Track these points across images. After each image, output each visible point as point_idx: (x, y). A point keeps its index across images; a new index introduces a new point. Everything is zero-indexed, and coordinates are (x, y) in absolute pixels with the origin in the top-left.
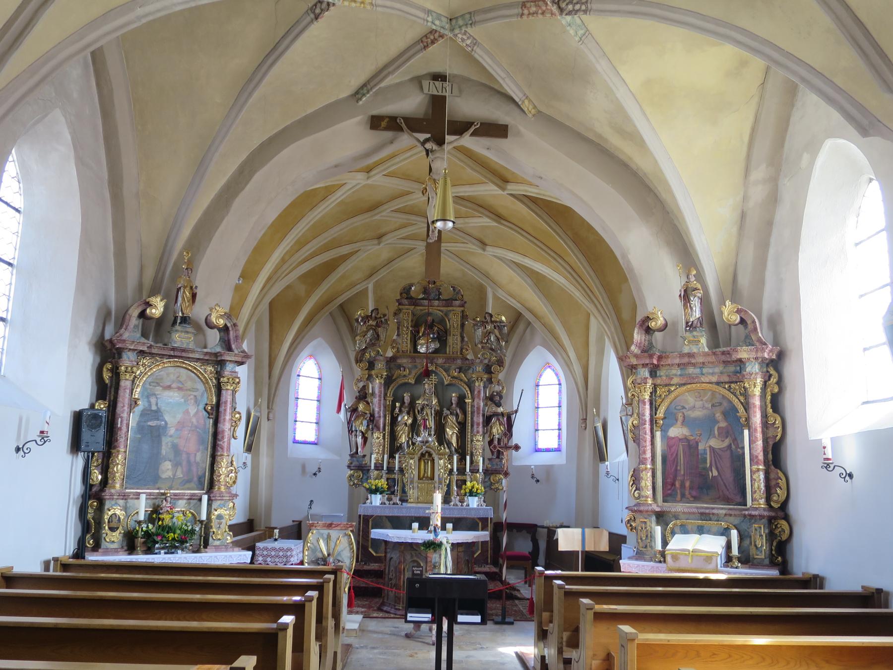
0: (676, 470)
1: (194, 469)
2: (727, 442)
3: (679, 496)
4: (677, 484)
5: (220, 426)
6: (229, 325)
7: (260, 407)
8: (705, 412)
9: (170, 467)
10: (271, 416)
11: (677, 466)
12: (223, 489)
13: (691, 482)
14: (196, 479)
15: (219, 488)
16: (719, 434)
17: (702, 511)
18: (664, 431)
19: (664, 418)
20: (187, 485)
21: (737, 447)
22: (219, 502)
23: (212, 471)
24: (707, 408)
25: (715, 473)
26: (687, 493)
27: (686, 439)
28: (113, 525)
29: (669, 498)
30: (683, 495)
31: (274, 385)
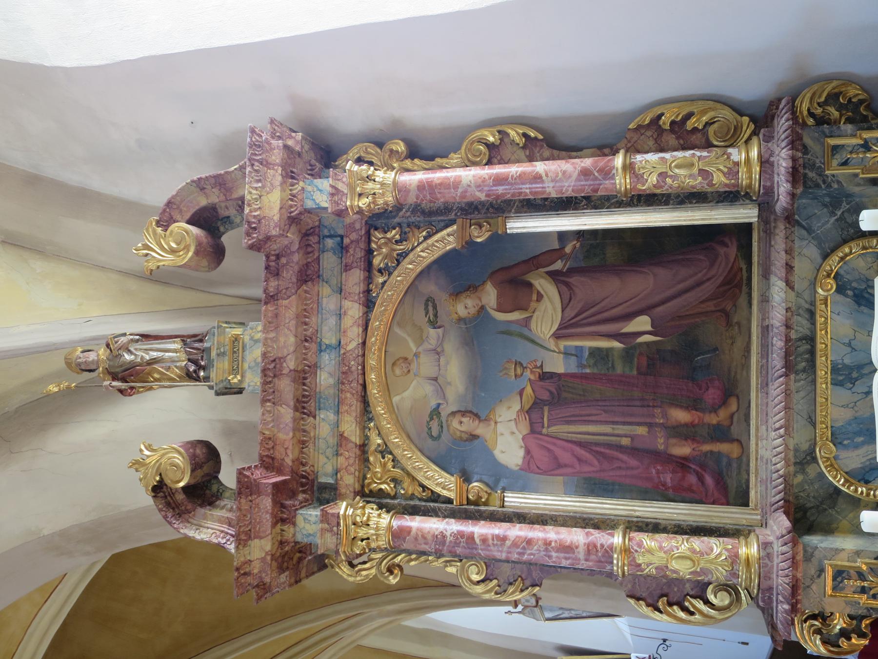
0: (633, 451)
2: (543, 284)
3: (723, 447)
4: (683, 450)
16: (524, 309)
17: (777, 361)
19: (466, 478)
21: (557, 254)
24: (441, 341)
25: (642, 323)
26: (712, 419)
27: (532, 412)
29: (732, 484)
30: (721, 434)
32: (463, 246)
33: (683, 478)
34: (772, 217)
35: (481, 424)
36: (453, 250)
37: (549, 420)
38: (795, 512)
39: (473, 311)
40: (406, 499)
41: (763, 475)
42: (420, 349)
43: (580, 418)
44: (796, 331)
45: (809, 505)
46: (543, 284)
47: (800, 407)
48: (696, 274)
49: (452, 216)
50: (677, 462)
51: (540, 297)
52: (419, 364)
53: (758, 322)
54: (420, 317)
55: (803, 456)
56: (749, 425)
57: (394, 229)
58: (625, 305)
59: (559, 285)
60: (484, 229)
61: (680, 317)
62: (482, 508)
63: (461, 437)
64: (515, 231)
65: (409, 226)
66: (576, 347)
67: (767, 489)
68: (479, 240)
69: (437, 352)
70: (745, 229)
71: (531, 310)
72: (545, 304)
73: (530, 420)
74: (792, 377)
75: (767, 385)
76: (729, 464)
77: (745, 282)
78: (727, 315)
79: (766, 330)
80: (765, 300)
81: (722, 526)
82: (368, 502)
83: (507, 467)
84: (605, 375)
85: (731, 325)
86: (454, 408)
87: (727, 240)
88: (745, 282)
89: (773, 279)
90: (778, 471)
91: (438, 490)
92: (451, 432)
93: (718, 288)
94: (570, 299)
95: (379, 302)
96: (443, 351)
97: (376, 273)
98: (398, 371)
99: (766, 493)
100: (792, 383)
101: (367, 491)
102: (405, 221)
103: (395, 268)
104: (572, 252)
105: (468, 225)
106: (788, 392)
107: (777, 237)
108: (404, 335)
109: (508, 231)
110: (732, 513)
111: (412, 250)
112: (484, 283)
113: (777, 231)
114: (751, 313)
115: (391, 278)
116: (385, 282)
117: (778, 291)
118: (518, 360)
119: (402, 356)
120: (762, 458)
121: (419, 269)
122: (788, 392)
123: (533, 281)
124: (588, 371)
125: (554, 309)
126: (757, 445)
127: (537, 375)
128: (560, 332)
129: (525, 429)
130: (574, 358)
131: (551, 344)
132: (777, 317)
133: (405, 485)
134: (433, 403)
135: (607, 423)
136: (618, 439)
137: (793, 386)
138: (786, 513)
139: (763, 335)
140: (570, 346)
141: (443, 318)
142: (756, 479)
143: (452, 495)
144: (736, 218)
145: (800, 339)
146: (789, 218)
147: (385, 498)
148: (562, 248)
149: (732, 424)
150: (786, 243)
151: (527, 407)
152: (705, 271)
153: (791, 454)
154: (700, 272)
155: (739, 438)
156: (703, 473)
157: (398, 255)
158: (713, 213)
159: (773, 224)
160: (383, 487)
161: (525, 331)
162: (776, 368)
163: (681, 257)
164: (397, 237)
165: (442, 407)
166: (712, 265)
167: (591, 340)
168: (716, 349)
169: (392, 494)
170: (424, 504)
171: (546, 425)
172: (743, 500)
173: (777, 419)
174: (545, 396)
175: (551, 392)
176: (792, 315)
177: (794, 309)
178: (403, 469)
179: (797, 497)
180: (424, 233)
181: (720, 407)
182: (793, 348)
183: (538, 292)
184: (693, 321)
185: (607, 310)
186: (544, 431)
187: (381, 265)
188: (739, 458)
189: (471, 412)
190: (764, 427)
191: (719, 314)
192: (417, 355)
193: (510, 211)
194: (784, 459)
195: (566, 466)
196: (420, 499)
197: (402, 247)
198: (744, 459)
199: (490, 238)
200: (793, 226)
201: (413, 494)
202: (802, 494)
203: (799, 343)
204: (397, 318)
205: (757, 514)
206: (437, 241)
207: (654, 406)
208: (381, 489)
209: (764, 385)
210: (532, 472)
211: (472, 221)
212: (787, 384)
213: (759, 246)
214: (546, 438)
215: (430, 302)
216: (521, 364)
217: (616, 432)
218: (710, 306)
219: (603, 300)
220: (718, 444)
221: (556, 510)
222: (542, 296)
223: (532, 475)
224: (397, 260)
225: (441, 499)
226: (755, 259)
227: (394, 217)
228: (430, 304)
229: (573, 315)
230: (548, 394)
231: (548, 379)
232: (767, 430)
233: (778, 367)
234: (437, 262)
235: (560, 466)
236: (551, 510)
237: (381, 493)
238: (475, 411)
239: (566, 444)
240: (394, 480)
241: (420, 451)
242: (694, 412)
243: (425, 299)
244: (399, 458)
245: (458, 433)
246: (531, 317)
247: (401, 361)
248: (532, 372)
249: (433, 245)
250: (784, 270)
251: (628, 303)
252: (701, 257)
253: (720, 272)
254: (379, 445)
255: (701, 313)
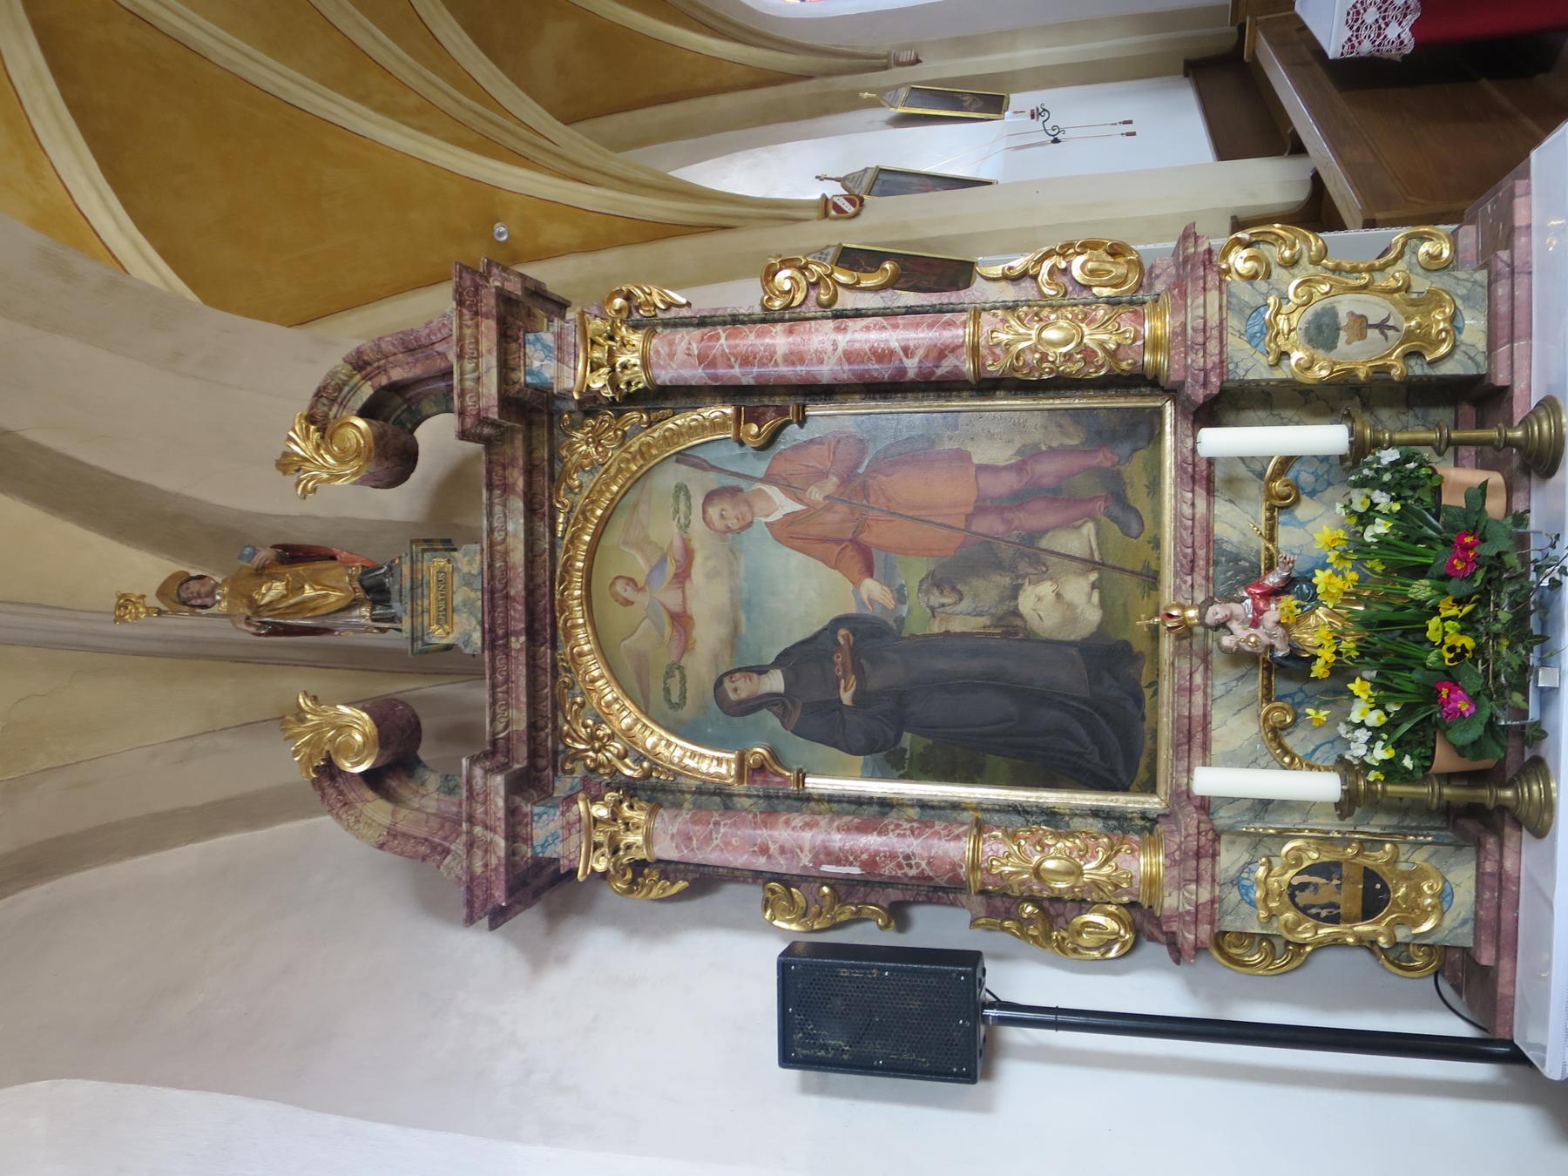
1: (1049, 469)
5: (826, 372)
6: (367, 391)
7: (882, 92)
9: (1046, 589)
10: (906, 56)
12: (1158, 325)
14: (1103, 459)
15: (1156, 345)
20: (1137, 496)
22: (1235, 344)
23: (1061, 384)
28: (1349, 896)
31: (826, 61)
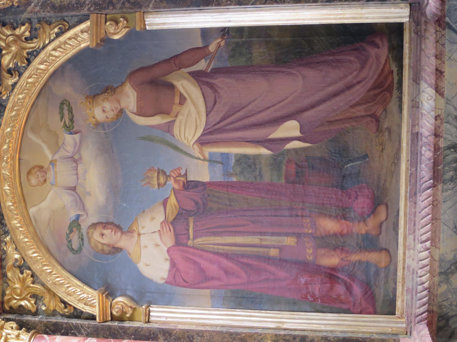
0: (281, 262)
2: (185, 86)
3: (372, 257)
4: (331, 260)
8: (89, 154)
11: (268, 259)
13: (324, 213)
16: (166, 112)
17: (425, 172)
18: (147, 294)
19: (110, 292)
21: (200, 52)
24: (78, 148)
25: (291, 128)
26: (360, 229)
27: (178, 223)
29: (380, 293)
30: (370, 243)
32: (98, 44)
33: (332, 288)
34: (423, 19)
35: (124, 237)
36: (87, 49)
37: (195, 231)
38: (439, 321)
39: (111, 115)
40: (48, 315)
41: (409, 284)
42: (57, 157)
43: (227, 229)
44: (445, 139)
45: (451, 314)
46: (185, 86)
47: (447, 217)
48: (346, 76)
49: (85, 11)
50: (326, 273)
51: (183, 100)
52: (56, 173)
53: (408, 128)
54: (55, 122)
55: (448, 266)
56: (397, 234)
57: (23, 24)
58: (272, 109)
59: (203, 87)
60: (120, 25)
61: (330, 122)
62: (127, 324)
63: (103, 250)
64: (155, 28)
65: (39, 22)
66: (222, 154)
67: (412, 298)
68: (116, 37)
69: (75, 160)
70: (396, 29)
71: (174, 113)
72: (189, 107)
73: (174, 232)
74: (440, 187)
75: (415, 194)
76: (377, 273)
77: (395, 85)
78: (377, 120)
79: (415, 137)
80: (415, 105)
81: (367, 336)
82: (8, 320)
83: (152, 281)
84: (252, 183)
85: (381, 131)
86: (94, 220)
87: (378, 40)
88: (395, 85)
89: (424, 85)
90: (423, 283)
91: (80, 306)
92: (93, 244)
93: (370, 90)
94: (215, 103)
95: (9, 106)
96: (81, 158)
97: (5, 74)
98: (34, 181)
99: (412, 302)
100: (439, 193)
101: (7, 308)
102: (35, 16)
103: (26, 68)
104: (217, 50)
105: (103, 21)
106: (435, 203)
107: (427, 41)
108: (39, 142)
109: (148, 28)
110: (378, 322)
111: (44, 47)
112: (123, 84)
113: (428, 35)
114: (401, 119)
115: (22, 79)
116: (16, 83)
117: (428, 98)
118: (161, 168)
119: (37, 164)
120: (409, 267)
121: (51, 70)
122: (435, 203)
123: (175, 83)
124: (234, 179)
125: (198, 113)
126: (404, 254)
127: (181, 184)
128: (204, 138)
129: (170, 241)
130: (219, 165)
131: (196, 151)
132: (427, 126)
133: (46, 300)
134: (72, 215)
135: (254, 233)
136: (266, 250)
137: (441, 196)
138: (429, 325)
139: (412, 140)
140: (214, 153)
141: (79, 122)
142: (403, 288)
143: (96, 311)
144: (387, 18)
145: (449, 148)
146: (440, 22)
147: (27, 314)
148: (207, 47)
149: (380, 233)
150: (436, 48)
151: (171, 218)
152: (355, 73)
153: (437, 264)
154: (350, 74)
155: (387, 247)
156: (352, 283)
157: (28, 54)
158: (364, 11)
159: (423, 27)
160: (23, 303)
161: (168, 137)
162: (424, 179)
163: (331, 58)
164: (27, 34)
165: (81, 218)
166: (362, 67)
167: (237, 147)
168: (366, 156)
169: (34, 310)
170: (66, 320)
171: (191, 237)
172: (390, 309)
173: (424, 232)
174: (190, 206)
175: (197, 203)
176: (442, 123)
177: (443, 116)
178: (43, 285)
179: (440, 307)
180: (56, 30)
181: (369, 216)
182: (441, 157)
183: (181, 95)
184: (342, 126)
185: (253, 115)
186: (190, 243)
187: (11, 65)
188: (387, 267)
189: (112, 223)
190: (412, 237)
191: (369, 119)
192: (53, 163)
193: (148, 6)
194: (430, 272)
195: (213, 278)
196: (62, 316)
197: (32, 45)
198: (392, 268)
199: (128, 35)
200: (444, 29)
201: (55, 311)
202: (445, 303)
203: (448, 152)
204: (31, 123)
205: (402, 323)
206: (70, 39)
207: (302, 216)
208: (21, 306)
209: (413, 194)
210: (178, 285)
211: (108, 16)
212: (434, 195)
213: (410, 47)
214: (191, 250)
215: (65, 105)
216: (164, 173)
217: (264, 243)
218: (360, 111)
219: (249, 104)
220: (367, 253)
221: (203, 325)
222: (185, 99)
223: (179, 288)
224: (27, 60)
225: (84, 316)
226: (406, 61)
227: (23, 12)
228: (65, 107)
229: (218, 120)
230: (193, 204)
231: (192, 188)
232: (414, 240)
233: (426, 178)
234: (69, 61)
235: (208, 279)
236: (198, 325)
237: (21, 310)
238: (117, 222)
239: (211, 256)
240: (34, 296)
241: (61, 265)
242: (343, 221)
243: (60, 101)
244: (38, 274)
245: (100, 246)
246: (174, 121)
247: (36, 170)
248: (176, 181)
249: (65, 43)
250: (433, 77)
251: (276, 107)
252: (352, 58)
253: (370, 74)
254: (16, 260)
255: (351, 118)
